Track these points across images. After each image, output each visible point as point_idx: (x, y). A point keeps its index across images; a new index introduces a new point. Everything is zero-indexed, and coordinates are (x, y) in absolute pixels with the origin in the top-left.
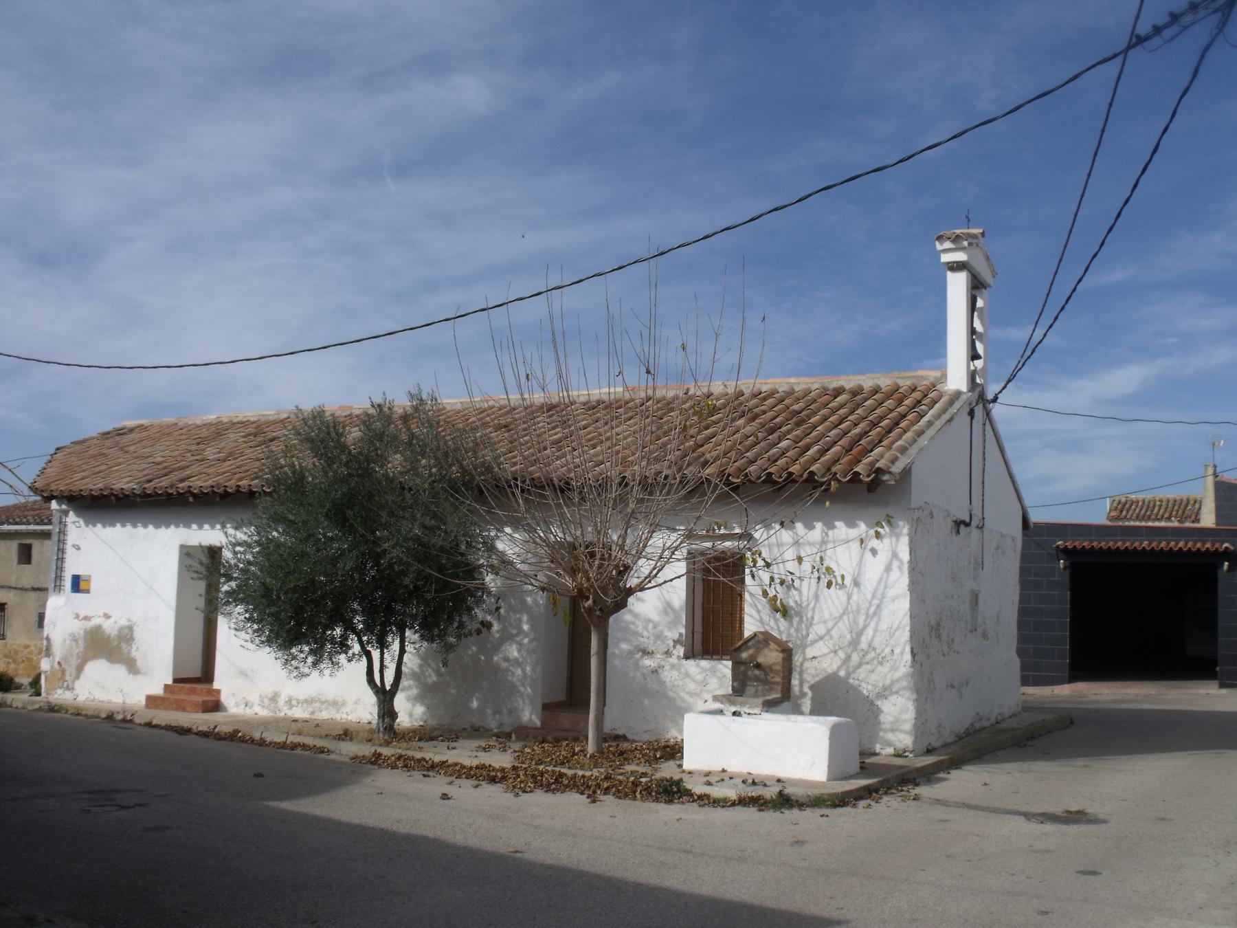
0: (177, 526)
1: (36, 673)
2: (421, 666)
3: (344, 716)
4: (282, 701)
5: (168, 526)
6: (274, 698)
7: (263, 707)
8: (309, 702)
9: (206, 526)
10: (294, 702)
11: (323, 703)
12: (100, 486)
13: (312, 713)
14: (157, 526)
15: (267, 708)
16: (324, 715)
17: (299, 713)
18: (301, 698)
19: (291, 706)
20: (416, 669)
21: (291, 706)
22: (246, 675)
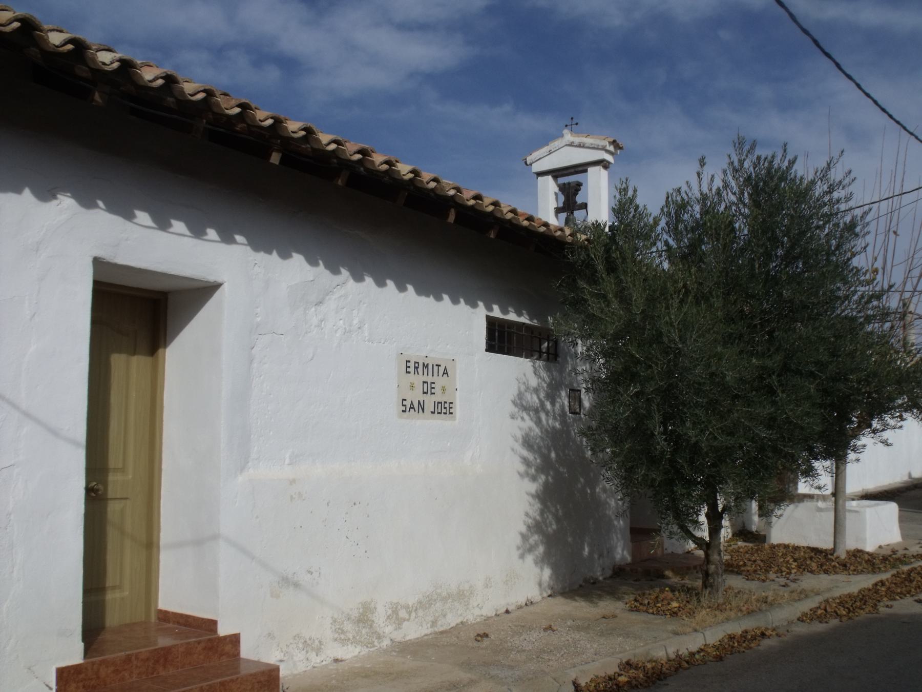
0: (87, 202)
1: (116, 49)
2: (542, 513)
3: (477, 612)
4: (380, 618)
5: (46, 194)
6: (364, 618)
7: (344, 642)
8: (425, 604)
9: (179, 226)
10: (403, 614)
11: (444, 600)
12: (671, 652)
13: (434, 623)
14: (257, 244)
15: (355, 641)
16: (451, 620)
17: (414, 631)
18: (412, 601)
19: (399, 623)
20: (538, 518)
21: (399, 623)
22: (296, 585)
